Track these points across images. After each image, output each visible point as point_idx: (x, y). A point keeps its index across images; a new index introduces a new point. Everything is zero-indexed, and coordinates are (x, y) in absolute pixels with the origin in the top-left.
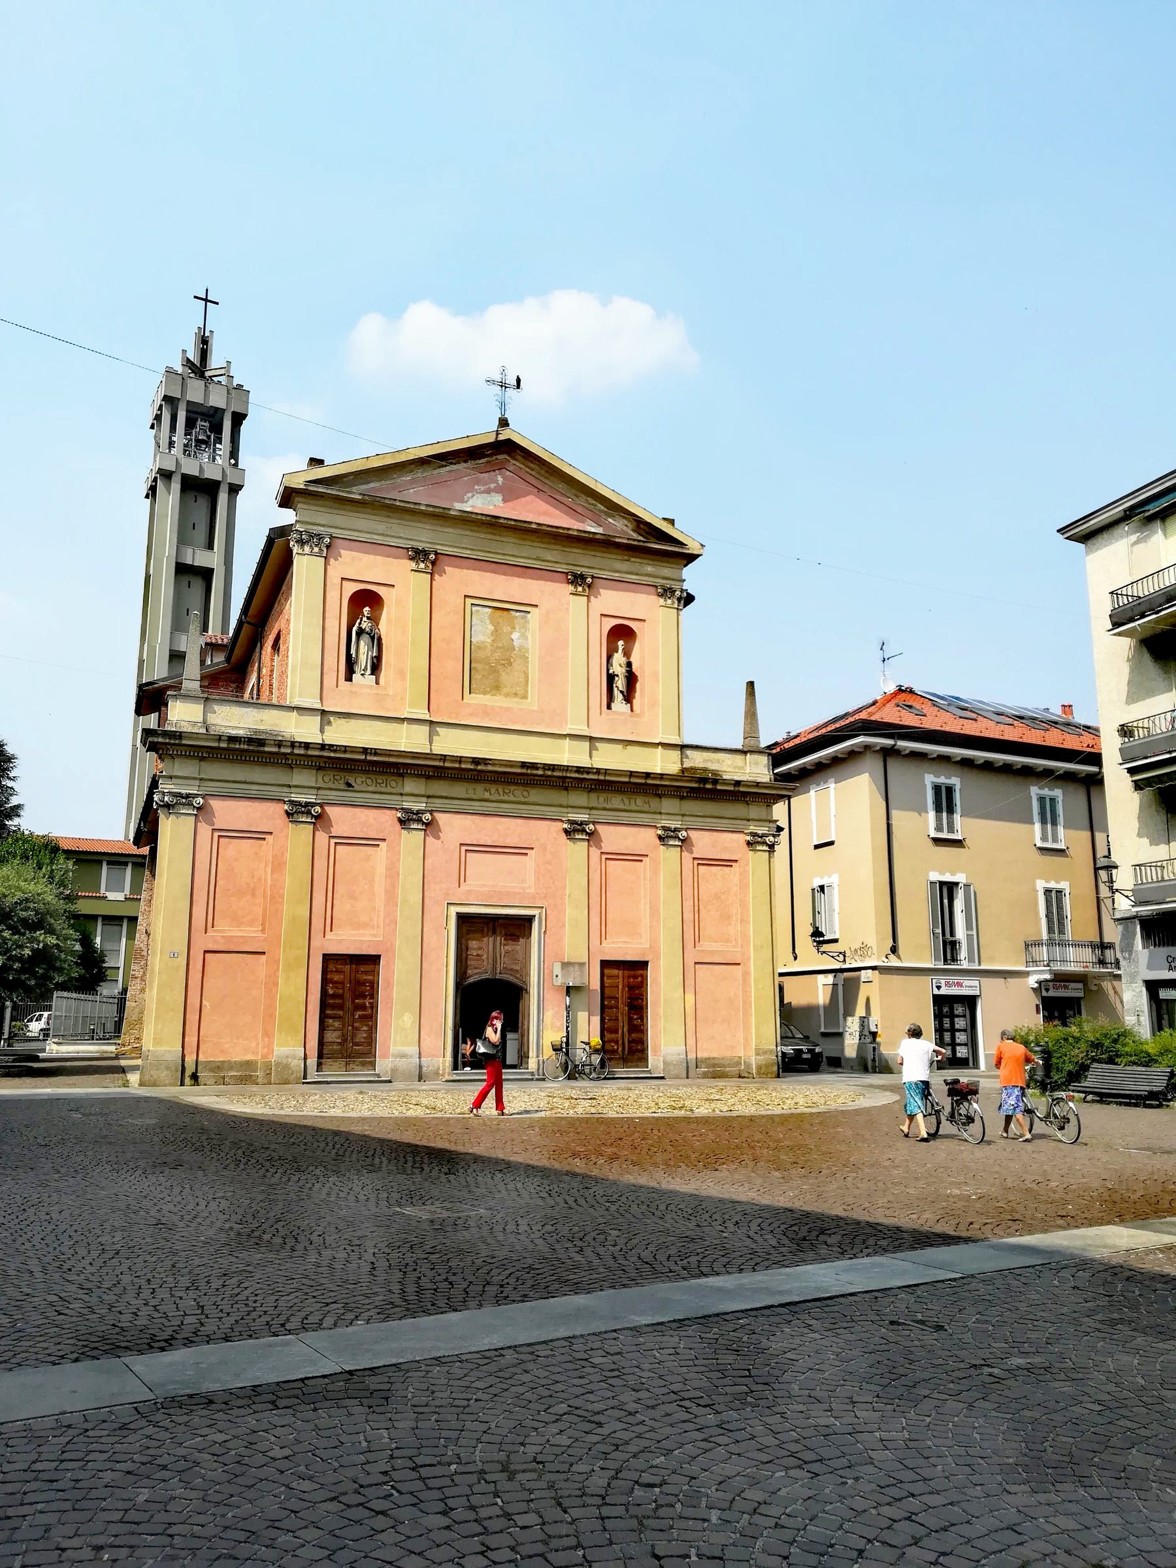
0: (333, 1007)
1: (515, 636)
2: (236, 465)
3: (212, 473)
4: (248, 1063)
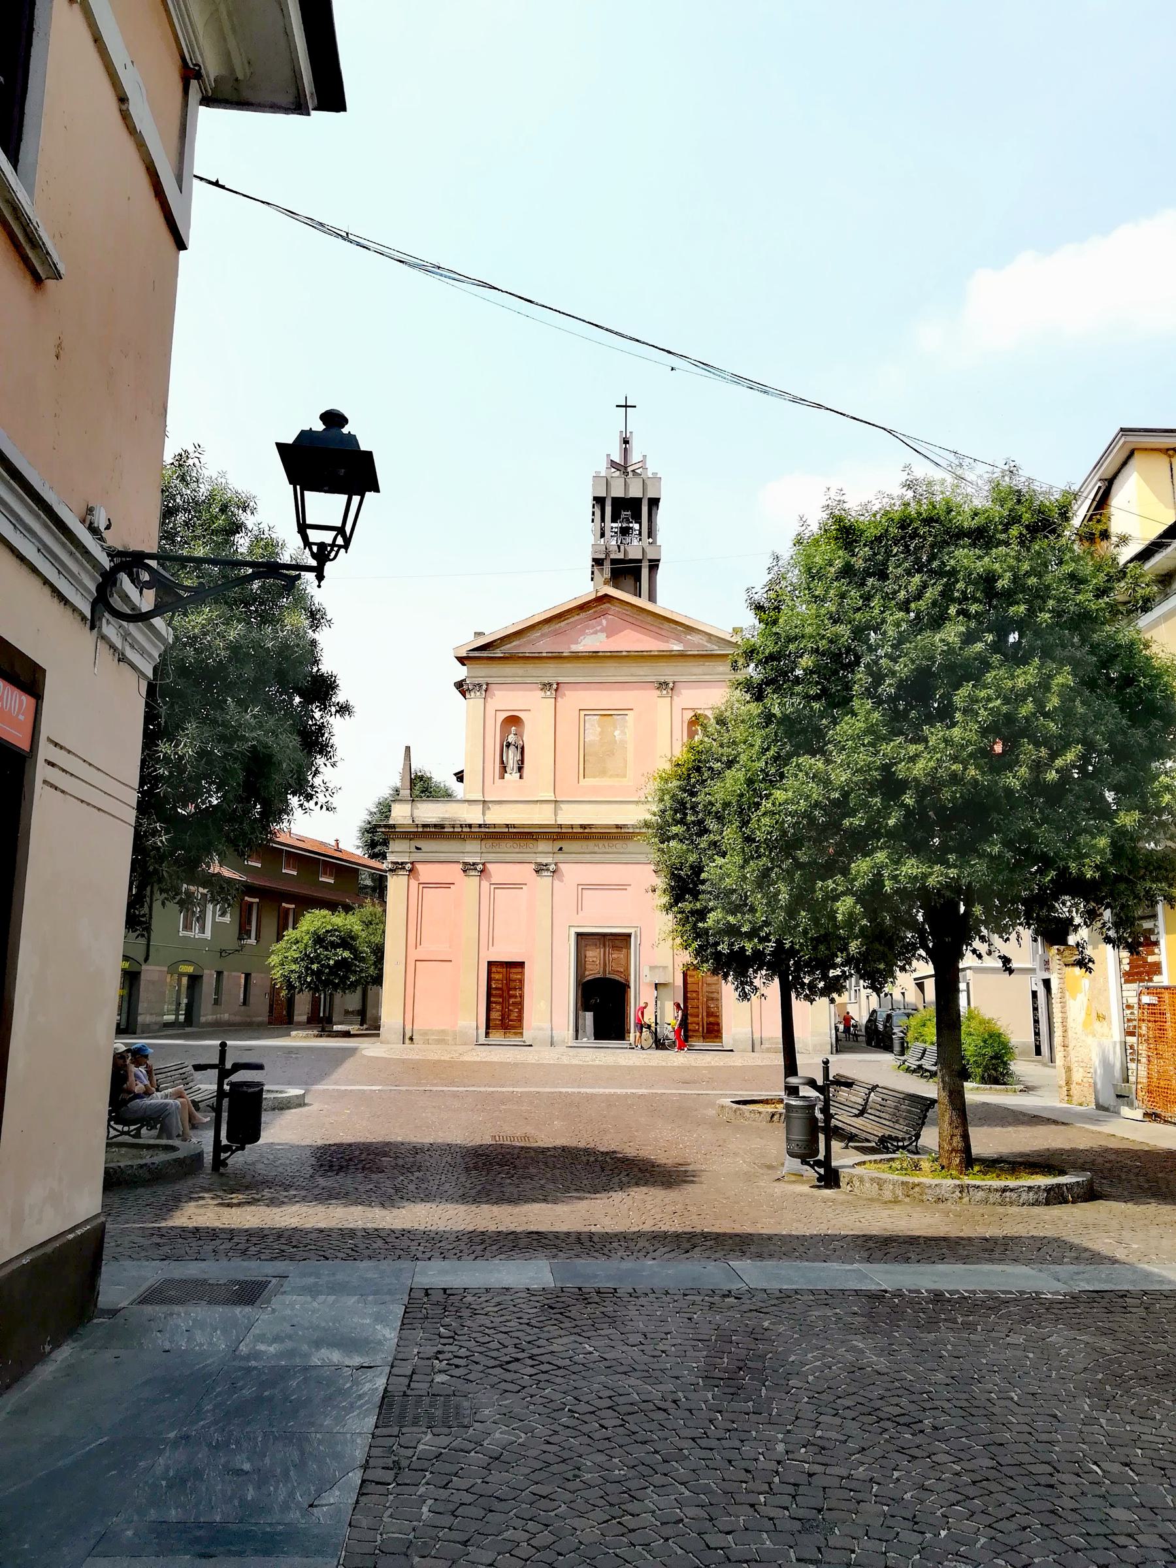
0: (496, 996)
1: (617, 733)
2: (654, 543)
3: (634, 554)
4: (443, 1031)
